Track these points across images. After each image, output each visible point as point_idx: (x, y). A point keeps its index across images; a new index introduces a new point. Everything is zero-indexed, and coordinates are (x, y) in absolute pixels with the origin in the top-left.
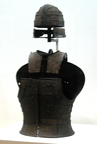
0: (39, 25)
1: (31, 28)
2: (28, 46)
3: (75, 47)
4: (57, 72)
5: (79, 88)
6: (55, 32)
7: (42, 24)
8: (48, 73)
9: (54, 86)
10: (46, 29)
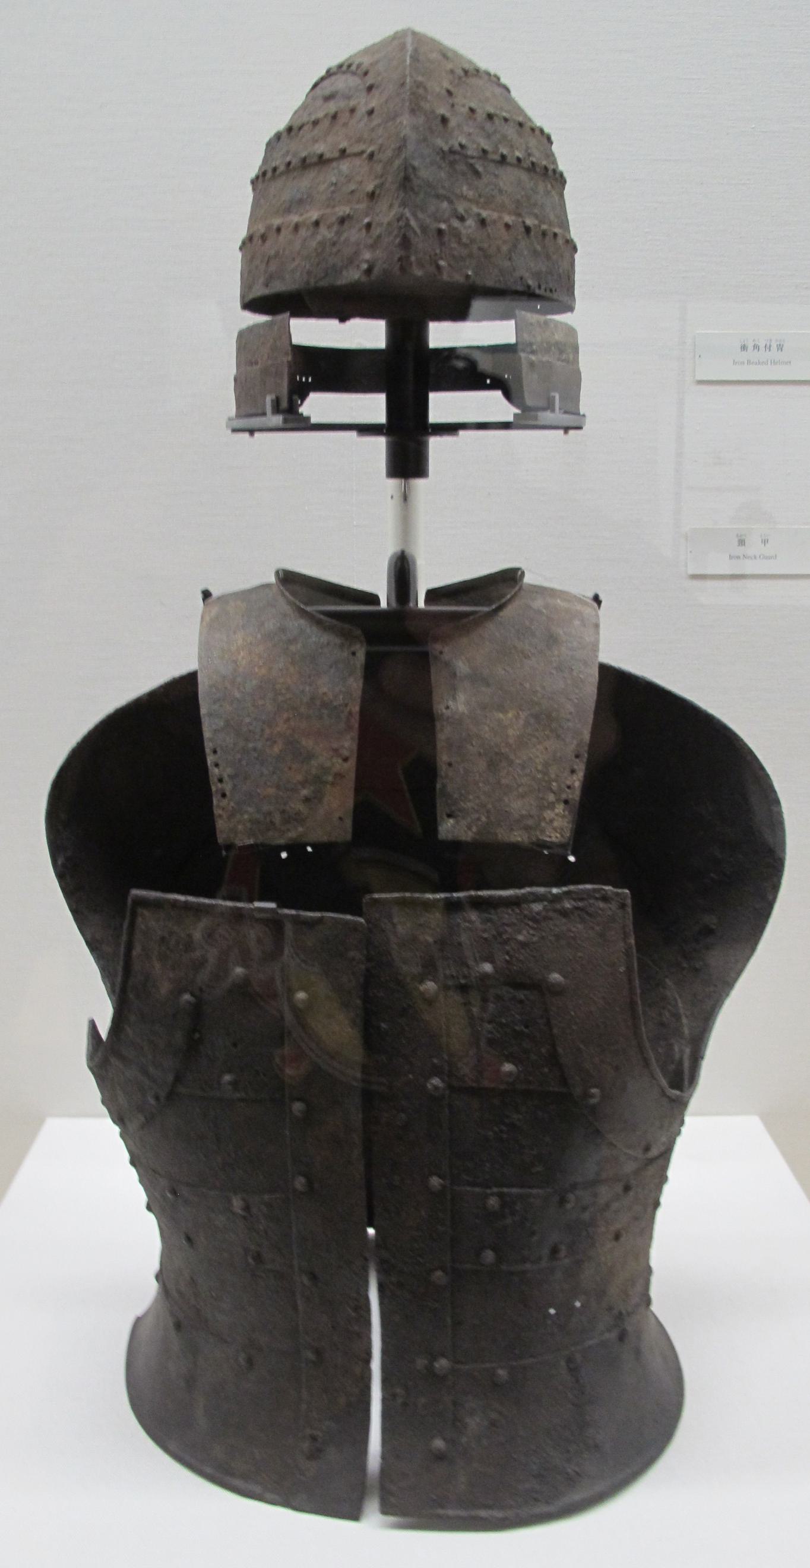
0: (353, 275)
1: (216, 322)
2: (177, 530)
3: (643, 513)
4: (557, 826)
5: (711, 920)
6: (532, 364)
7: (404, 263)
8: (456, 845)
9: (556, 977)
10: (368, 334)
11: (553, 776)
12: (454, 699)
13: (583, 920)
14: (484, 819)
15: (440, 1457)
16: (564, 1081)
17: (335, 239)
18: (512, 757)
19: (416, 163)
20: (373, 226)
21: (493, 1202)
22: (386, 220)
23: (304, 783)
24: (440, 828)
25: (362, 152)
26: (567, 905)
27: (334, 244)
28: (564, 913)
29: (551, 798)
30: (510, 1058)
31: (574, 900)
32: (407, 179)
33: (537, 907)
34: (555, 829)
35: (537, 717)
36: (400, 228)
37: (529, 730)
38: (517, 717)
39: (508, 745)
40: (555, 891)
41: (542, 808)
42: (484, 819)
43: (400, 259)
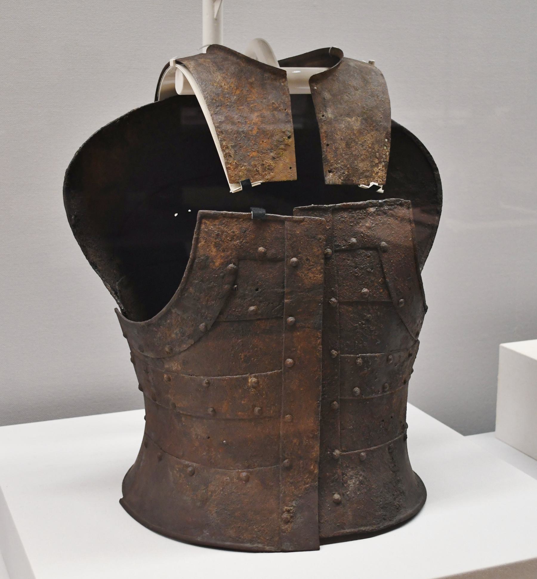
9: (383, 243)
11: (376, 150)
12: (326, 112)
14: (346, 173)
15: (338, 503)
16: (389, 295)
18: (357, 140)
21: (359, 361)
23: (271, 150)
24: (326, 178)
29: (377, 161)
31: (389, 205)
33: (372, 210)
34: (379, 177)
37: (363, 126)
38: (357, 120)
39: (354, 134)
40: (380, 201)
41: (373, 166)
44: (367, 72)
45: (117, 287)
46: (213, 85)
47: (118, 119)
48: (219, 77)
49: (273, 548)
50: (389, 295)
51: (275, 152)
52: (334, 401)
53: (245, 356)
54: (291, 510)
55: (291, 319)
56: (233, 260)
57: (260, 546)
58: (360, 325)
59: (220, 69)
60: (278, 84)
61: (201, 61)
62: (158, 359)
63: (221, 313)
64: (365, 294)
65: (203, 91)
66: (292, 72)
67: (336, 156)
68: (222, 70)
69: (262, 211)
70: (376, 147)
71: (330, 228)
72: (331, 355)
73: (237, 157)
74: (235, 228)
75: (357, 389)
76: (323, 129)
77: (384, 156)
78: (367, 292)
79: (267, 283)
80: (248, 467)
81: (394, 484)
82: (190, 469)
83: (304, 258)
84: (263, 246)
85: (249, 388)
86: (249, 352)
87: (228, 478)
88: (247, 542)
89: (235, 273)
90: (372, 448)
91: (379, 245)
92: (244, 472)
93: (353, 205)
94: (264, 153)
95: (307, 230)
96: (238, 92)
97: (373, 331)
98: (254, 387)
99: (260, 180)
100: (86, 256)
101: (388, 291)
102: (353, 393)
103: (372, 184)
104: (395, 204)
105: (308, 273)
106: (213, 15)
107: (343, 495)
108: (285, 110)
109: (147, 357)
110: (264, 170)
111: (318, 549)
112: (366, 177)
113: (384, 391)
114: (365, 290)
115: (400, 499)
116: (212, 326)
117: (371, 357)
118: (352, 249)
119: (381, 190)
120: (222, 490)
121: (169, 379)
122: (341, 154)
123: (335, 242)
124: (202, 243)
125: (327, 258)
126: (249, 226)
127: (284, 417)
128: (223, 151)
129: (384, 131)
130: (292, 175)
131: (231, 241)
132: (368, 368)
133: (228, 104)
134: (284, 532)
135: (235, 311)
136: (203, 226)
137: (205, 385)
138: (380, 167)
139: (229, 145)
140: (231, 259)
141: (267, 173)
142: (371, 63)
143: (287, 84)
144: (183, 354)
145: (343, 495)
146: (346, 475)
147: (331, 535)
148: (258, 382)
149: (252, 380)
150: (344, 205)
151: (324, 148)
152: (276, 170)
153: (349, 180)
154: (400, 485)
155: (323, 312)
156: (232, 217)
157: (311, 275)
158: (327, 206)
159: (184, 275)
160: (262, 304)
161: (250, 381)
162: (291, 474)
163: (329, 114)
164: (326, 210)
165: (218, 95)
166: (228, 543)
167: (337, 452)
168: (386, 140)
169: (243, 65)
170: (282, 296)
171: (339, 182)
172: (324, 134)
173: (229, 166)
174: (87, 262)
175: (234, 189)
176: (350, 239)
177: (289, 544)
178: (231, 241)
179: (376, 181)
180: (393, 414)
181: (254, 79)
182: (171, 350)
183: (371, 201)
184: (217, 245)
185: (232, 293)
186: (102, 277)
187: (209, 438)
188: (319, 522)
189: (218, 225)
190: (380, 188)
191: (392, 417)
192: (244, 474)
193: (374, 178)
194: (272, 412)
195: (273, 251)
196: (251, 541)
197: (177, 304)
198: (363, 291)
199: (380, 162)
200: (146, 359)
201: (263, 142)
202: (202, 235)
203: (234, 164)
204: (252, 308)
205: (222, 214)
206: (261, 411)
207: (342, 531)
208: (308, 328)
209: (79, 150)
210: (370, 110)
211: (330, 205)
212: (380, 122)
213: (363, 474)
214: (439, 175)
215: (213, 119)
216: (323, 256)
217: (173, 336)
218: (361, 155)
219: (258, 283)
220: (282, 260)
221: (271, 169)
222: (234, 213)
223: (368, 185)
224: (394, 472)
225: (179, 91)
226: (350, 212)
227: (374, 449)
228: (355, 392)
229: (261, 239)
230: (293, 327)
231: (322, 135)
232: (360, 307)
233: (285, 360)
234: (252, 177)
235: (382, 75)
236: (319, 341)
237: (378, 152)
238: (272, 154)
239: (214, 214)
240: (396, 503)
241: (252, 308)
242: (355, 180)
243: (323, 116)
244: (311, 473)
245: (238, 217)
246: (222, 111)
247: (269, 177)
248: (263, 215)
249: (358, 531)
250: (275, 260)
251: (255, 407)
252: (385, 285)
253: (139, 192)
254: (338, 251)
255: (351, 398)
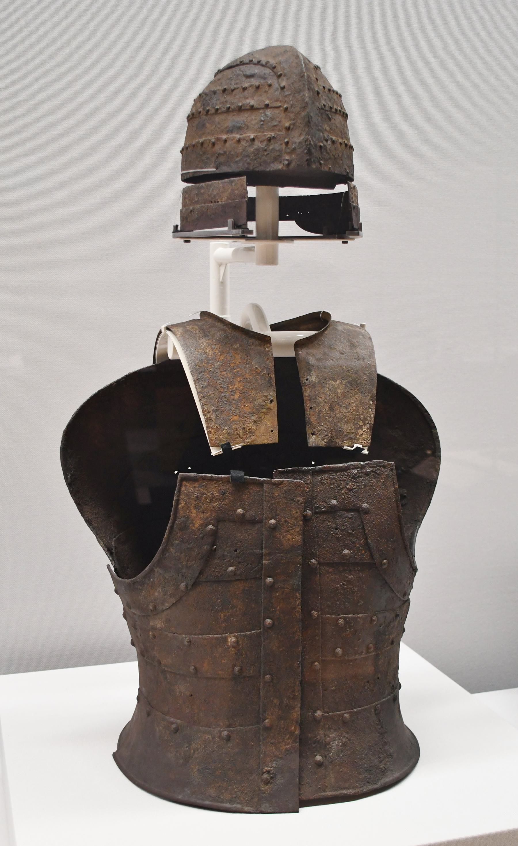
3: (386, 296)
9: (365, 505)
11: (361, 412)
12: (310, 375)
13: (375, 477)
14: (330, 435)
15: (320, 765)
16: (372, 556)
17: (266, 148)
19: (312, 115)
20: (290, 144)
21: (341, 622)
22: (298, 141)
23: (253, 414)
24: (309, 441)
25: (280, 107)
26: (368, 470)
27: (265, 150)
28: (367, 474)
29: (361, 423)
30: (347, 547)
32: (309, 122)
33: (355, 471)
34: (363, 439)
35: (350, 383)
36: (307, 145)
38: (341, 383)
39: (338, 397)
40: (362, 463)
41: (357, 429)
42: (330, 435)
43: (307, 160)
44: (356, 336)
45: (113, 543)
46: (198, 352)
47: (114, 382)
48: (205, 344)
49: (251, 809)
50: (372, 556)
51: (257, 416)
52: (315, 662)
53: (225, 616)
54: (271, 770)
55: (269, 580)
56: (212, 522)
57: (239, 806)
58: (341, 586)
59: (205, 336)
60: (262, 349)
61: (189, 327)
62: (144, 616)
63: (201, 573)
64: (345, 555)
65: (188, 357)
66: (276, 336)
67: (319, 418)
68: (208, 336)
69: (240, 474)
70: (361, 409)
71: (309, 490)
72: (311, 615)
73: (218, 422)
74: (214, 490)
75: (339, 650)
76: (307, 392)
77: (369, 419)
78: (348, 553)
79: (246, 545)
80: (229, 726)
81: (381, 747)
82: (174, 726)
83: (283, 520)
84: (241, 508)
85: (229, 648)
86: (228, 612)
87: (210, 736)
88: (226, 802)
89: (214, 534)
90: (356, 710)
91: (360, 507)
92: (225, 730)
93: (333, 467)
94: (246, 417)
95: (286, 492)
96: (222, 358)
97: (355, 592)
98: (233, 647)
99: (241, 443)
100: (81, 513)
101: (370, 552)
102: (335, 655)
103: (356, 446)
104: (378, 466)
105: (286, 535)
106: (219, 278)
107: (326, 757)
108: (269, 374)
109: (134, 614)
110: (245, 433)
111: (297, 811)
112: (351, 439)
113: (368, 652)
114: (346, 551)
115: (387, 762)
116: (192, 586)
117: (352, 618)
118: (332, 511)
119: (366, 452)
120: (204, 748)
121: (154, 637)
122: (325, 417)
123: (314, 504)
124: (182, 504)
125: (306, 519)
126: (228, 488)
127: (264, 677)
128: (205, 415)
129: (369, 393)
130: (274, 438)
131: (210, 503)
132: (350, 629)
133: (211, 369)
134: (264, 793)
135: (214, 571)
136: (183, 489)
137: (186, 643)
138: (365, 429)
139: (211, 410)
140: (211, 520)
141: (247, 436)
142: (362, 326)
143: (272, 349)
144: (165, 613)
145: (326, 757)
146: (329, 737)
147: (312, 798)
148: (237, 642)
149: (232, 639)
150: (325, 468)
151: (308, 411)
152: (258, 434)
153: (332, 442)
154: (387, 747)
155: (302, 573)
156: (211, 479)
157: (289, 537)
158: (307, 468)
159: (165, 536)
160: (241, 565)
161: (229, 640)
162: (271, 735)
163: (313, 378)
164: (305, 473)
165: (202, 361)
166: (207, 803)
167: (319, 713)
168: (371, 402)
169: (229, 331)
170: (261, 557)
171: (322, 444)
172: (307, 397)
173: (210, 430)
174: (82, 519)
175: (215, 451)
176: (330, 501)
177: (267, 805)
178: (210, 503)
179: (362, 444)
180: (379, 675)
181: (238, 345)
182: (155, 607)
183: (352, 463)
184: (196, 507)
185: (211, 555)
186: (96, 534)
187: (192, 695)
188: (300, 783)
189: (198, 488)
190: (363, 449)
191: (378, 678)
192: (225, 733)
193: (358, 440)
194: (251, 672)
195: (251, 513)
196: (230, 801)
197: (159, 564)
198: (344, 552)
199: (364, 424)
200: (135, 616)
201: (244, 406)
202: (182, 497)
203: (215, 427)
204: (231, 569)
205: (202, 477)
206: (241, 671)
207: (324, 794)
208: (288, 588)
209: (77, 412)
210: (355, 373)
211: (310, 468)
212: (365, 384)
213: (346, 735)
214: (437, 433)
215: (195, 385)
216: (302, 518)
217: (156, 594)
218: (345, 417)
219: (236, 544)
220: (260, 522)
221: (252, 433)
222: (213, 475)
223: (352, 447)
224: (381, 734)
225: (170, 356)
226: (331, 474)
227: (359, 710)
228: (337, 653)
229: (239, 501)
230: (272, 587)
231: (305, 398)
232: (341, 569)
233: (264, 620)
234: (233, 440)
235: (370, 338)
236: (298, 602)
237: (362, 414)
238: (253, 418)
239: (194, 477)
240: (382, 766)
241: (231, 569)
242: (338, 442)
243: (307, 380)
244: (292, 733)
245: (217, 480)
246: (204, 377)
247: (249, 441)
248: (242, 477)
249: (340, 794)
250: (253, 522)
251: (235, 666)
252: (367, 546)
253: (129, 452)
254: (318, 512)
255: (333, 659)
